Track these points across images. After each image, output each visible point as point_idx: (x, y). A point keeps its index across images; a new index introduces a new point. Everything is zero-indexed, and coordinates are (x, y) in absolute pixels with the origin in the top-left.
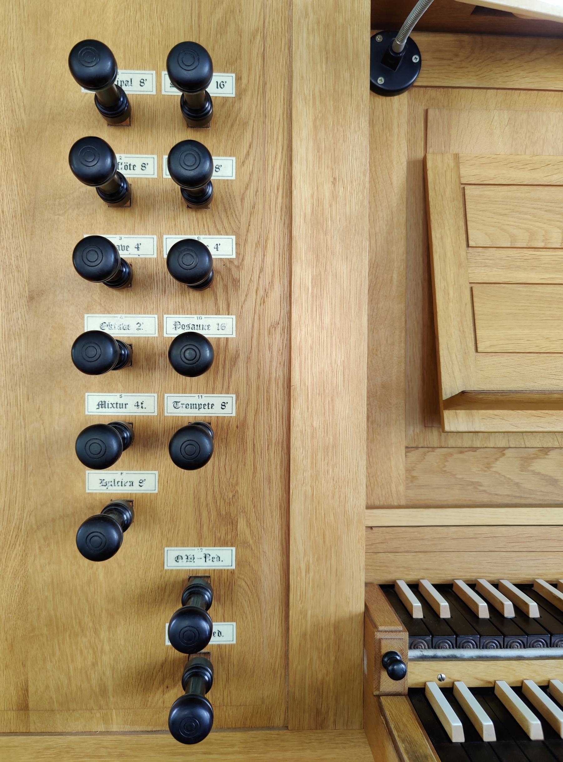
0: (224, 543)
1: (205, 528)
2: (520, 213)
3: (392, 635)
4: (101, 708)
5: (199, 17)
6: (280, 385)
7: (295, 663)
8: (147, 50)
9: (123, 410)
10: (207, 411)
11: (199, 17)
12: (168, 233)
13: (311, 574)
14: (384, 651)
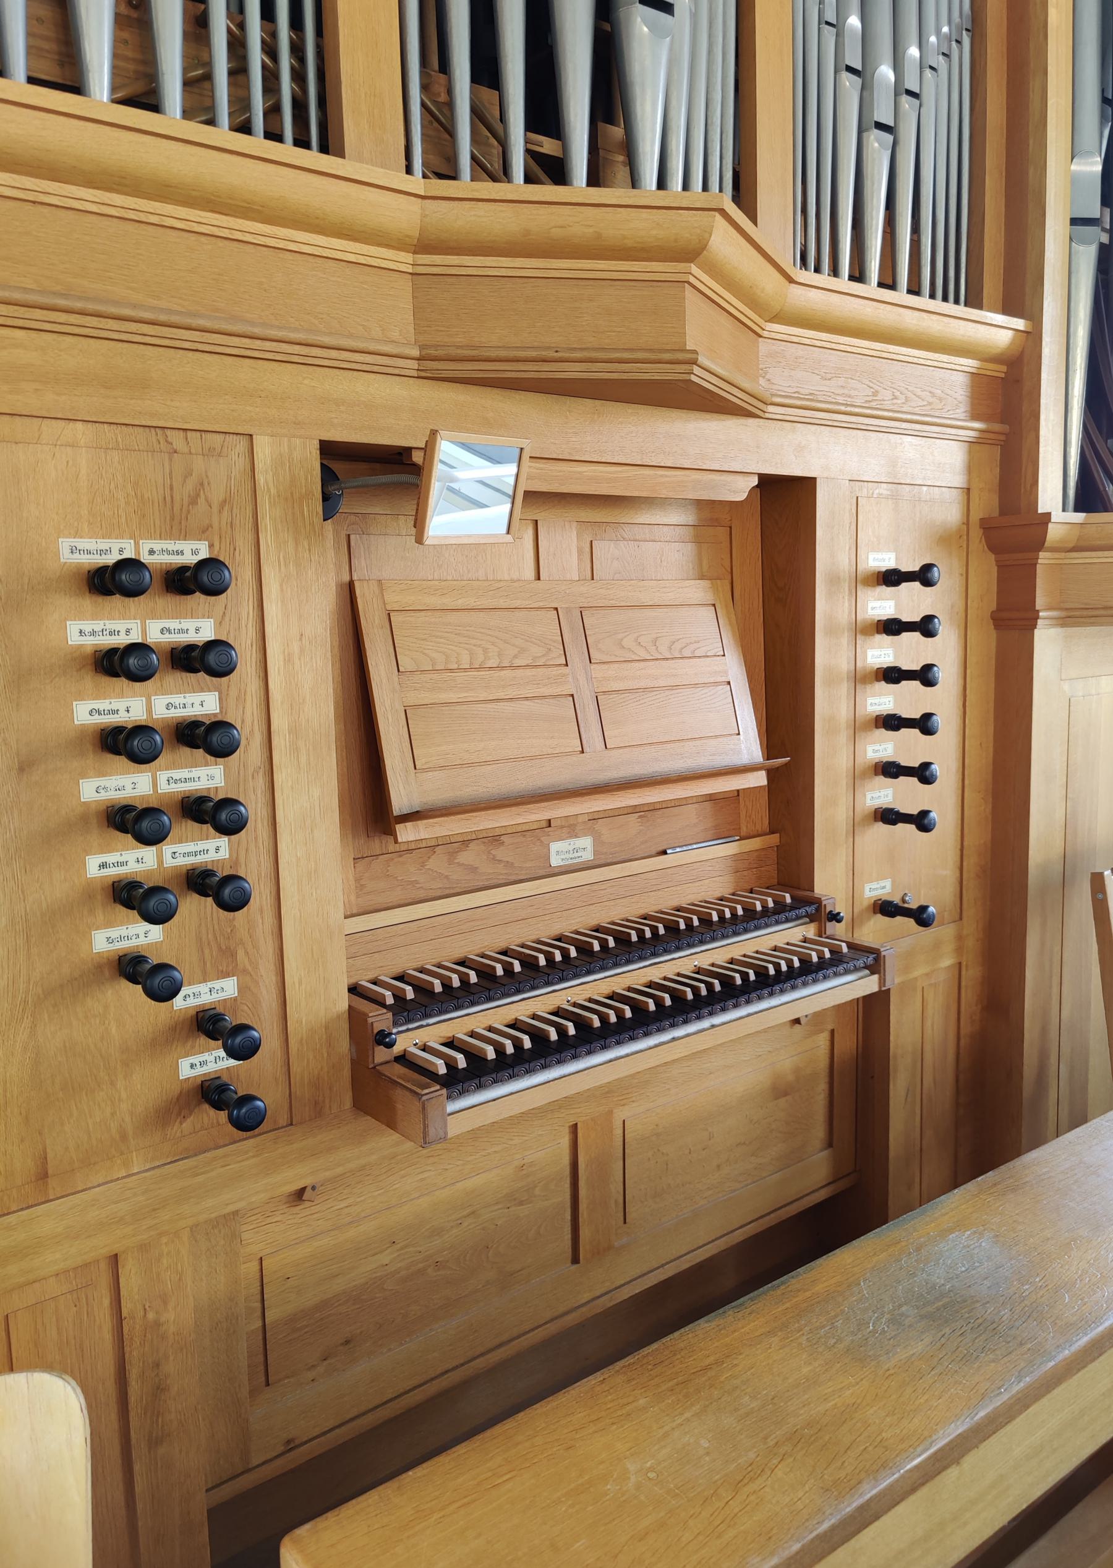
0: (226, 975)
1: (208, 964)
2: (437, 637)
3: (380, 1020)
4: (122, 1153)
5: (171, 488)
6: (265, 823)
7: (295, 1068)
8: (123, 520)
9: (125, 867)
10: (203, 856)
11: (171, 488)
12: (156, 694)
13: (303, 986)
14: (375, 1031)
